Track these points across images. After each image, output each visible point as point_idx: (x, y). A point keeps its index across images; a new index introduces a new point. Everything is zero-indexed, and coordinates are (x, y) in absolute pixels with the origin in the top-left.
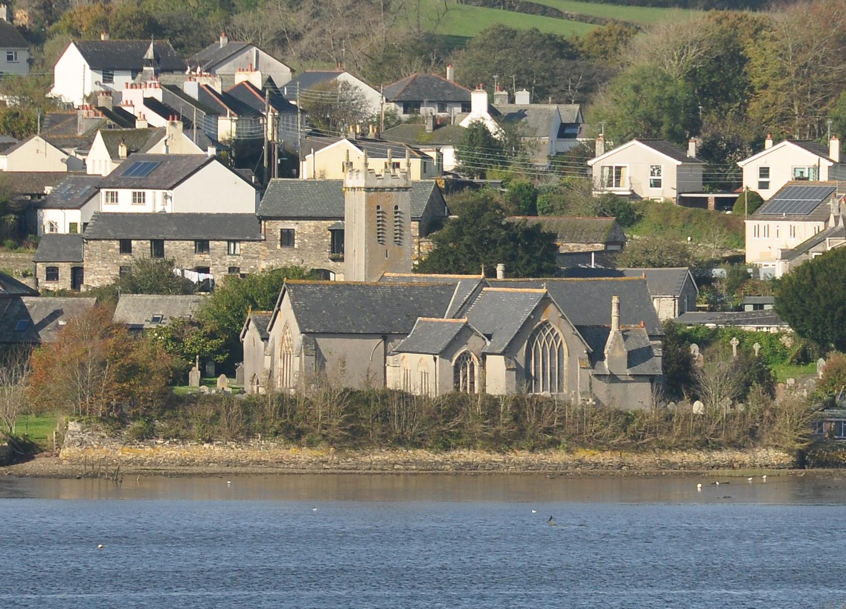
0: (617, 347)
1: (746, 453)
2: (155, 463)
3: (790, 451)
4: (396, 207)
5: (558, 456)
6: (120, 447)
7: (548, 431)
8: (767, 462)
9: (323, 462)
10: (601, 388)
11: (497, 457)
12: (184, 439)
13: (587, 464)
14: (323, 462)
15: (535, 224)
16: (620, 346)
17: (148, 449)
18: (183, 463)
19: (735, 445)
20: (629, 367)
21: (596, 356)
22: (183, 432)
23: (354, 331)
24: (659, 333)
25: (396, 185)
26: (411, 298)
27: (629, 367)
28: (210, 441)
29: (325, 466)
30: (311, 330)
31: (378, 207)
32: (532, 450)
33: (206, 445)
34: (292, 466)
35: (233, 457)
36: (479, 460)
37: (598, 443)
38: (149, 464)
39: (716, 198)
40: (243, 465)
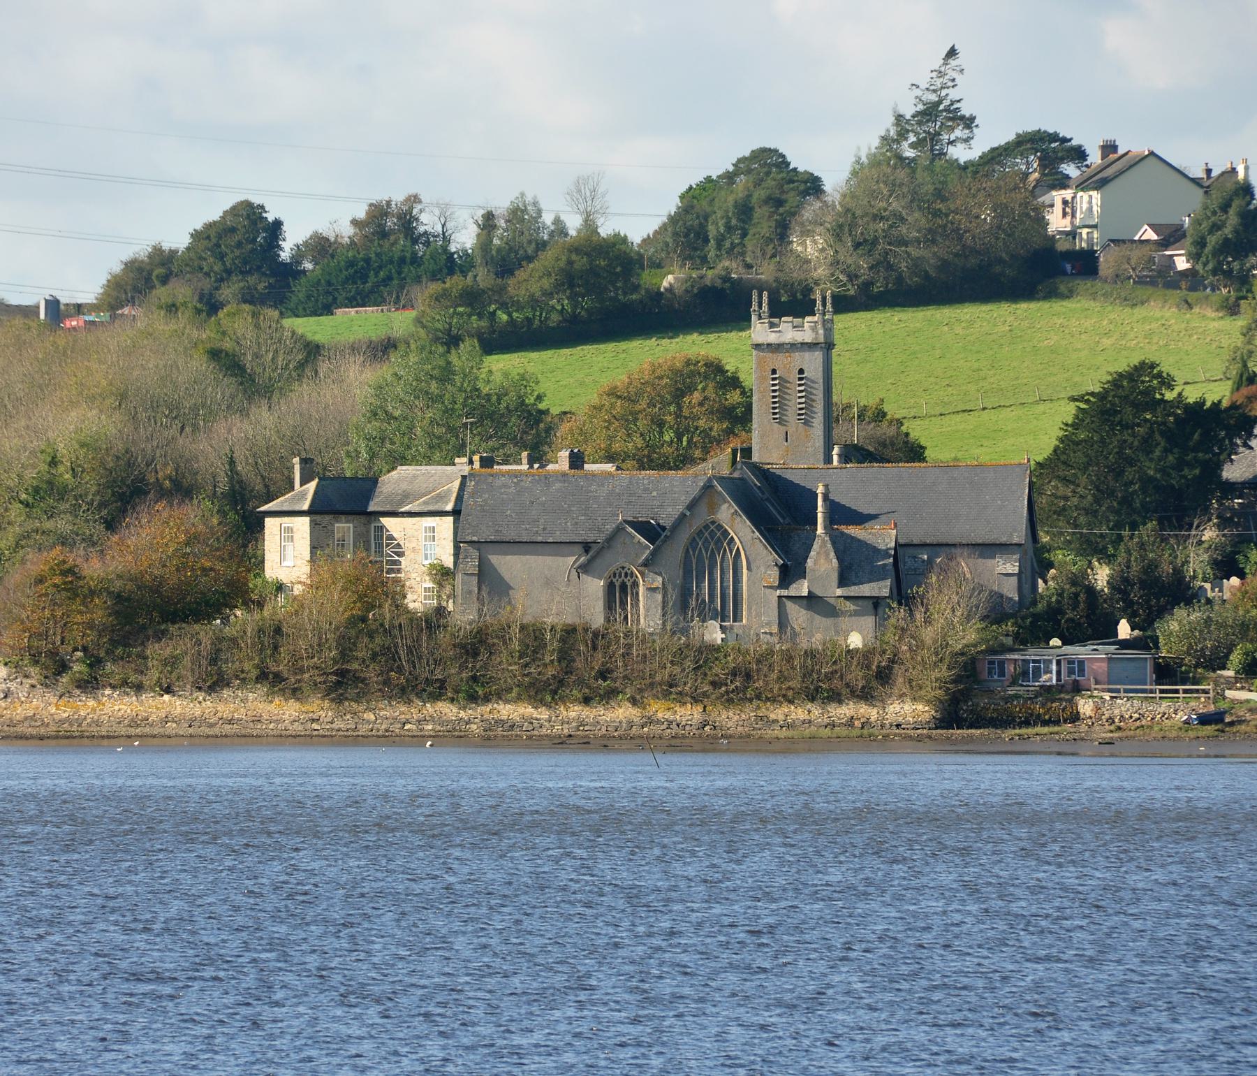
0: (823, 557)
1: (874, 706)
2: (98, 723)
3: (928, 702)
4: (801, 371)
5: (621, 711)
6: (54, 700)
7: (603, 675)
8: (900, 719)
9: (313, 720)
10: (798, 616)
11: (543, 714)
12: (139, 688)
13: (659, 722)
14: (313, 720)
15: (514, 374)
16: (827, 555)
17: (91, 703)
18: (134, 723)
19: (865, 695)
20: (842, 582)
21: (790, 572)
22: (133, 678)
23: (539, 539)
24: (1016, 540)
25: (800, 340)
26: (654, 494)
27: (842, 582)
28: (168, 690)
29: (315, 726)
30: (475, 539)
31: (774, 372)
32: (587, 701)
33: (166, 697)
34: (271, 726)
35: (198, 713)
36: (515, 717)
37: (670, 690)
38: (89, 725)
39: (38, 307)
40: (211, 726)
